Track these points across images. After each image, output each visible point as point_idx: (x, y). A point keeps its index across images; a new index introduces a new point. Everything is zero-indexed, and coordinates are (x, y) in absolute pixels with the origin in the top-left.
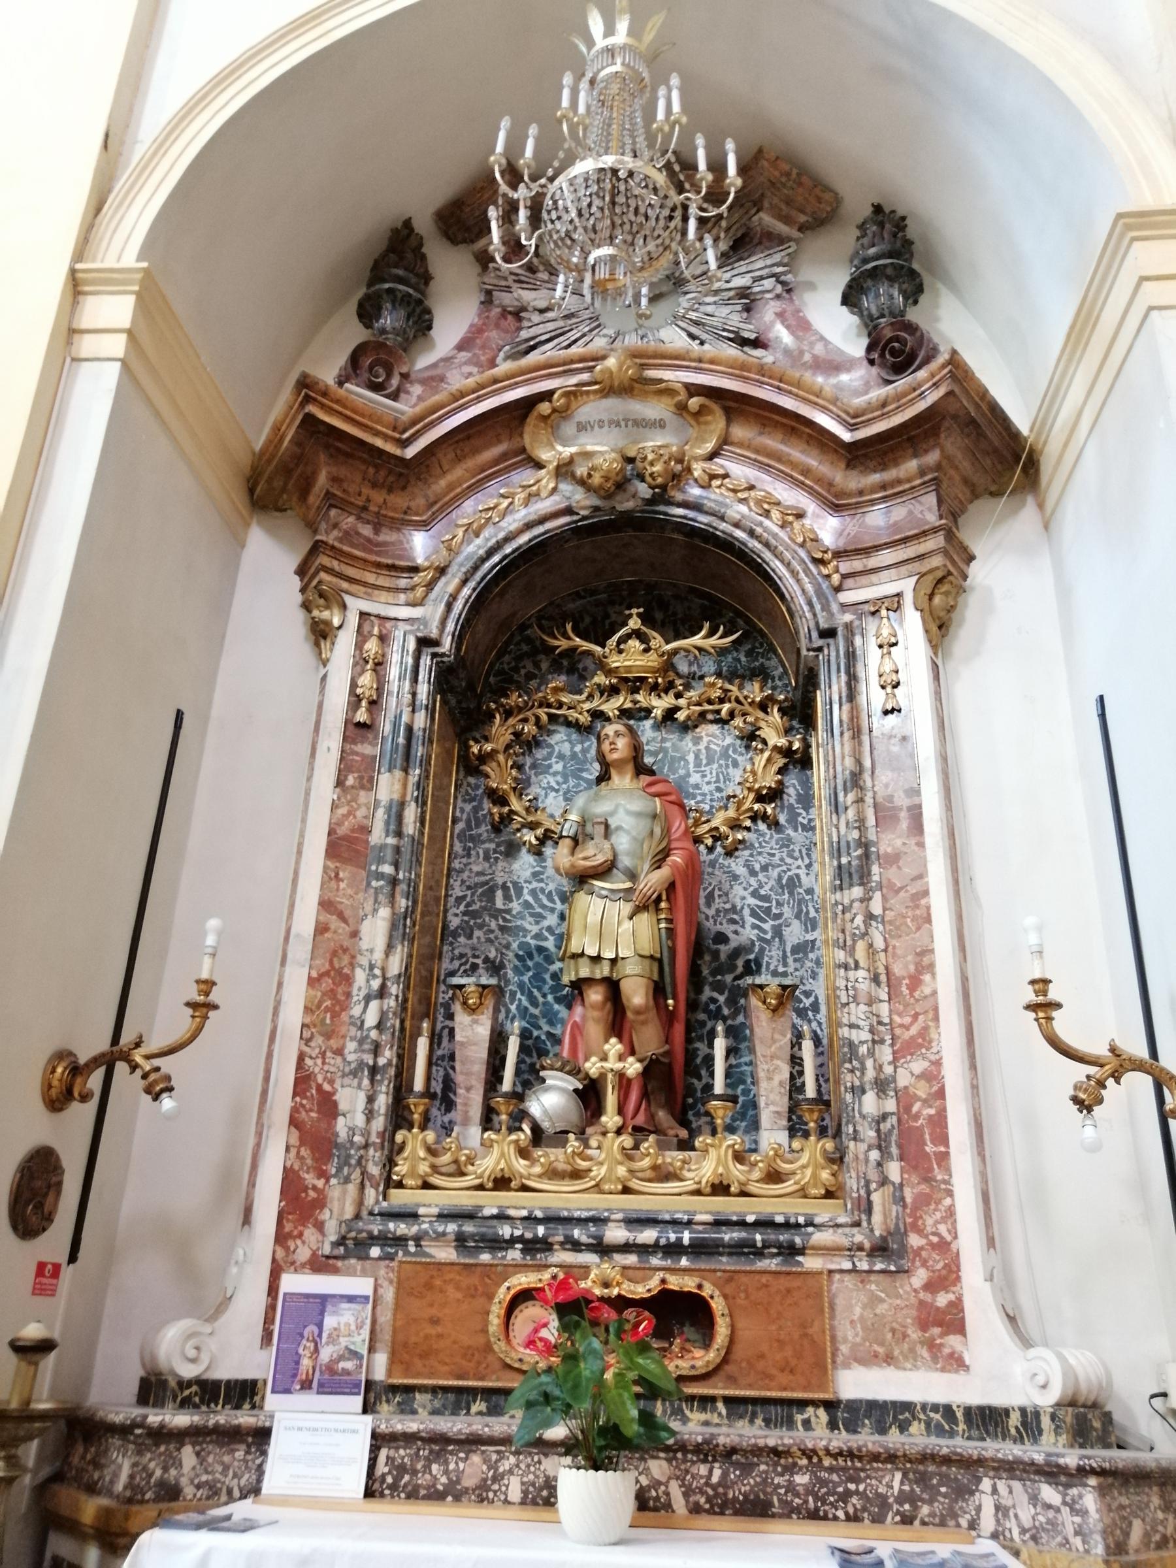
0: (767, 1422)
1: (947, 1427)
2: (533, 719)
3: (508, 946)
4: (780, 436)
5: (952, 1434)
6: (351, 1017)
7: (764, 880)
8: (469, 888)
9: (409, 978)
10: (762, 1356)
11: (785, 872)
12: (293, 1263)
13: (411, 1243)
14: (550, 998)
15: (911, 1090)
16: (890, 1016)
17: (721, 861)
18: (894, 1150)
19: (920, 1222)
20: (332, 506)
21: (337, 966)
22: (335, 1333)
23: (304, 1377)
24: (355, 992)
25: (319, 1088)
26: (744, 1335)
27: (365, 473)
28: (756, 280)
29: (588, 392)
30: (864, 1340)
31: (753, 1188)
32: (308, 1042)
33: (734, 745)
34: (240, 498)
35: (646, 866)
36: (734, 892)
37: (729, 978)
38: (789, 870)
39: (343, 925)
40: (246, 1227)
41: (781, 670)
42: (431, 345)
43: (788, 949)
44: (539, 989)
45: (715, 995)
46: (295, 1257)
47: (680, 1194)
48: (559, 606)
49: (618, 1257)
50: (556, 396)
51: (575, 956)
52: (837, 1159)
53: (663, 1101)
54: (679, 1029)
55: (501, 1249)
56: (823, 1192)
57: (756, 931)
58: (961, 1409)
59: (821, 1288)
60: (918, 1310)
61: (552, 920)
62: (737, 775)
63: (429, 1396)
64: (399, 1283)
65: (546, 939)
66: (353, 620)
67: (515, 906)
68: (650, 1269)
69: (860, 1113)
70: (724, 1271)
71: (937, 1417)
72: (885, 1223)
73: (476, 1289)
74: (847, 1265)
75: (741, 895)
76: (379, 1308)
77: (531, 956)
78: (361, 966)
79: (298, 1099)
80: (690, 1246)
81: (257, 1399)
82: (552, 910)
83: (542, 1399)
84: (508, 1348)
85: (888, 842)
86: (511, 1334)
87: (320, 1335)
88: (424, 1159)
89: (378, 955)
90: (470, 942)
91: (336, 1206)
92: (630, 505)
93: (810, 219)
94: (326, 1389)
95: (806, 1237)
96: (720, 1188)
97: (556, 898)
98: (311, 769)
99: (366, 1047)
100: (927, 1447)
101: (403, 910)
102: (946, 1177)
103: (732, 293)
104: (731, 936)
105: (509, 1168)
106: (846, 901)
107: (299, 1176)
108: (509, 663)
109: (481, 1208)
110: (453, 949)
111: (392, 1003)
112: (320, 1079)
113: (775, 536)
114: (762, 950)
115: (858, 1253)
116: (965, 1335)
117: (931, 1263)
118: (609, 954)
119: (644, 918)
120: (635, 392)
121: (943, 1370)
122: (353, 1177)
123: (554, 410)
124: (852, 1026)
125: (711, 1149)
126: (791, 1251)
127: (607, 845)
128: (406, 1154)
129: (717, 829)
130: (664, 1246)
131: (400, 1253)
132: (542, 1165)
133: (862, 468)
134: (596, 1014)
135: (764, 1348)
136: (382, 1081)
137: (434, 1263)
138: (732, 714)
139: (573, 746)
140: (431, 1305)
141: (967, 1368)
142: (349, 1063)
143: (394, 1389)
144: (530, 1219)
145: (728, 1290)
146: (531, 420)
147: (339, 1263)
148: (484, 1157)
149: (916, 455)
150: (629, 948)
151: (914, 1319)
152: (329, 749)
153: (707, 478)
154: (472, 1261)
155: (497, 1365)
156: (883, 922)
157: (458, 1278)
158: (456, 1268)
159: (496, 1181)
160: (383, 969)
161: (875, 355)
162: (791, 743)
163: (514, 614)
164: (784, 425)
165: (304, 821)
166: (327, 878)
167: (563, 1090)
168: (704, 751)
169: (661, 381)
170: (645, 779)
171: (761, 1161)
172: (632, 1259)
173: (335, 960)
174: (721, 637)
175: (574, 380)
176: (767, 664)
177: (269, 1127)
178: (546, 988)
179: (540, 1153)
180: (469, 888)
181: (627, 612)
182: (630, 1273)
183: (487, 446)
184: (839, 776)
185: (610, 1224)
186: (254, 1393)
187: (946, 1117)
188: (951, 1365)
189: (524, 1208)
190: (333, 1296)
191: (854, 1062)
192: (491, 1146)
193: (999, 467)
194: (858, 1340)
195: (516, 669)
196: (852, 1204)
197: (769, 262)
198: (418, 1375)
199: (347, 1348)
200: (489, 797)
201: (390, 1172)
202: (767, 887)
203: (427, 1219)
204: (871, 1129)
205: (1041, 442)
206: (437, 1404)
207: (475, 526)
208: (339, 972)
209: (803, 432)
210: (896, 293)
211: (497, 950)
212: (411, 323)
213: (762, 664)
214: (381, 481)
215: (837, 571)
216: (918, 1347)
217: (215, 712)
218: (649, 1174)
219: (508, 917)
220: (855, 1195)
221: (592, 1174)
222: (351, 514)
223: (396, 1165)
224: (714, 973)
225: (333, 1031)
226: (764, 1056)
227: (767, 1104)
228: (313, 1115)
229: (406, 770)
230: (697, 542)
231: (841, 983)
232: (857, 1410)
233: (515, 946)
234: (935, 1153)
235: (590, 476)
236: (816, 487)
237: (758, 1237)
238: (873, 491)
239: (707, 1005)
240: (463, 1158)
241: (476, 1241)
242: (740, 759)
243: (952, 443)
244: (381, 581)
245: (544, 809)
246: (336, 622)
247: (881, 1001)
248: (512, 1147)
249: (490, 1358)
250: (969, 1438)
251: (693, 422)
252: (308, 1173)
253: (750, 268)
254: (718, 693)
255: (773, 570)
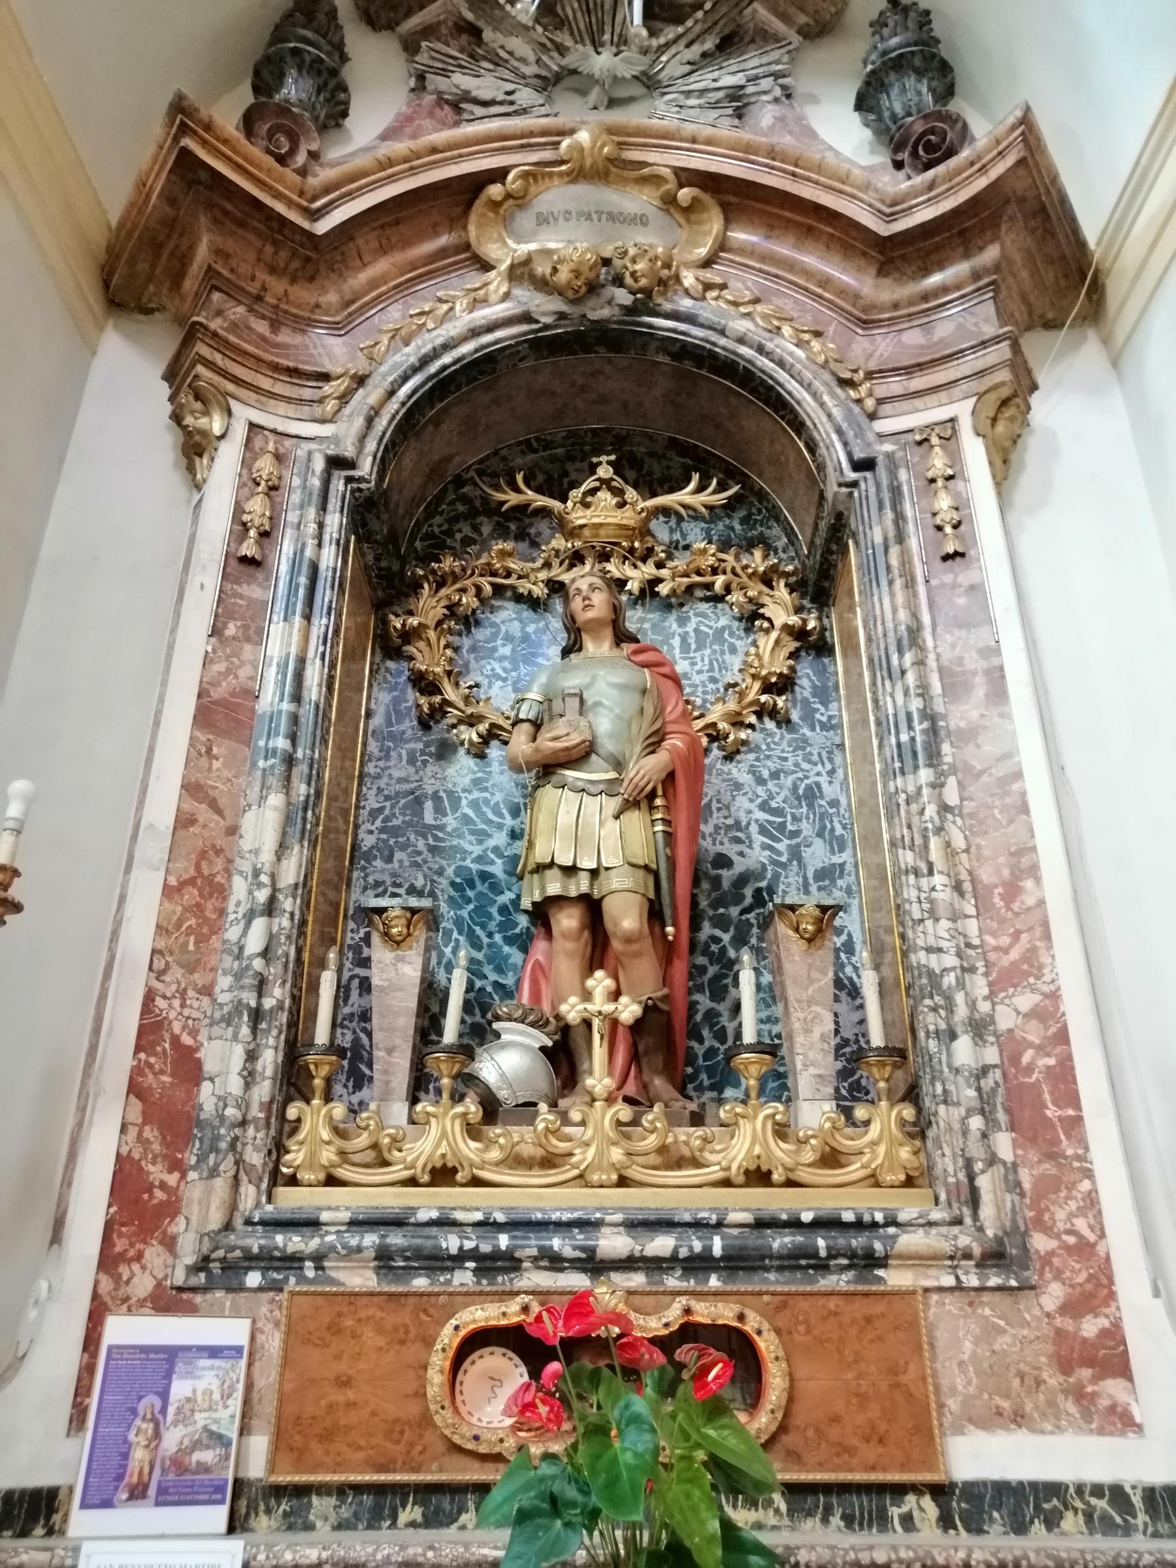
0: (849, 1520)
1: (1118, 1520)
2: (473, 591)
3: (440, 872)
4: (792, 240)
5: (1127, 1530)
6: (225, 942)
7: (774, 789)
8: (387, 798)
9: (310, 892)
10: (835, 1419)
11: (801, 780)
12: (126, 1299)
13: (309, 1264)
14: (498, 938)
15: (1018, 1034)
16: (980, 936)
17: (718, 766)
18: (1001, 1116)
19: (1046, 1217)
20: (215, 288)
21: (206, 872)
22: (188, 1406)
23: (135, 1479)
24: (231, 907)
25: (175, 1040)
26: (809, 1388)
27: (260, 251)
28: (754, 79)
29: (551, 175)
30: (981, 1389)
31: (803, 1175)
32: (160, 975)
33: (730, 627)
34: (94, 298)
35: (638, 749)
36: (737, 804)
37: (734, 911)
38: (807, 777)
39: (216, 817)
40: (55, 1246)
41: (785, 540)
42: (349, 139)
43: (810, 875)
44: (483, 926)
45: (718, 932)
46: (129, 1290)
47: (700, 1186)
48: (504, 459)
49: (617, 1277)
50: (510, 177)
51: (540, 868)
52: (919, 1130)
53: (661, 1067)
54: (680, 968)
55: (444, 1269)
56: (902, 1177)
57: (767, 853)
58: (1139, 1492)
59: (915, 1314)
60: (1055, 1343)
61: (499, 839)
62: (736, 662)
63: (333, 1501)
64: (289, 1325)
65: (492, 863)
66: (239, 431)
67: (451, 822)
68: (664, 1293)
69: (949, 1066)
70: (774, 1294)
71: (1101, 1504)
72: (999, 1218)
73: (407, 1332)
74: (948, 1281)
75: (745, 808)
76: (257, 1364)
77: (472, 886)
78: (241, 873)
79: (142, 1056)
80: (723, 1258)
81: (56, 1518)
82: (500, 827)
83: (545, 1506)
84: (457, 1420)
85: (958, 716)
86: (459, 1398)
87: (164, 1411)
88: (328, 1143)
89: (267, 857)
90: (389, 866)
91: (194, 1212)
92: (605, 313)
93: (811, 22)
94: (167, 1497)
95: (890, 1242)
96: (759, 1177)
97: (505, 811)
98: (177, 614)
99: (247, 981)
100: (1118, 1555)
101: (302, 798)
102: (1080, 1152)
103: (721, 94)
104: (736, 858)
105: (454, 1154)
106: (911, 789)
107: (141, 1169)
108: (440, 526)
109: (413, 1210)
110: (366, 876)
111: (286, 923)
112: (177, 1027)
113: (791, 354)
114: (776, 876)
115: (963, 1263)
116: (1130, 1379)
117: (1068, 1274)
118: (589, 863)
119: (635, 819)
120: (612, 177)
121: (1101, 1432)
122: (222, 1168)
123: (509, 196)
124: (929, 950)
125: (741, 1121)
126: (869, 1262)
127: (583, 723)
128: (301, 1136)
129: (713, 725)
130: (686, 1259)
131: (292, 1280)
132: (501, 1147)
133: (897, 275)
134: (570, 945)
135: (838, 1406)
136: (269, 1030)
137: (343, 1294)
138: (728, 589)
139: (524, 625)
140: (338, 1357)
141: (1138, 1428)
142: (221, 1005)
143: (278, 1491)
144: (487, 1225)
145: (782, 1321)
146: (478, 207)
147: (198, 1299)
148: (416, 1140)
149: (967, 255)
150: (616, 856)
151: (1049, 1357)
152: (202, 586)
153: (700, 287)
154: (400, 1289)
155: (440, 1447)
156: (961, 815)
157: (379, 1314)
158: (376, 1299)
159: (433, 1171)
160: (273, 876)
161: (905, 156)
162: (805, 621)
163: (448, 459)
164: (797, 224)
165: (164, 683)
166: (194, 753)
167: (526, 1048)
168: (692, 634)
169: (644, 164)
170: (628, 648)
171: (813, 1137)
172: (637, 1280)
173: (204, 865)
174: (714, 493)
175: (534, 157)
176: (767, 532)
177: (97, 1096)
178: (492, 926)
179: (498, 1131)
180: (387, 798)
181: (595, 460)
182: (637, 1300)
183: (421, 237)
184: (891, 634)
185: (604, 1230)
186: (51, 1510)
187: (1072, 1068)
188: (1114, 1424)
189: (477, 1209)
190: (187, 1349)
191: (937, 998)
192: (428, 1123)
193: (1063, 283)
194: (972, 1390)
195: (450, 533)
196: (948, 1193)
197: (765, 60)
198: (316, 1468)
199: (205, 1429)
200: (414, 686)
201: (277, 1162)
202: (779, 799)
203: (333, 1229)
204: (970, 1087)
205: (1111, 258)
206: (346, 1512)
207: (403, 332)
208: (210, 880)
209: (821, 232)
210: (925, 90)
211: (425, 877)
212: (321, 98)
213: (761, 533)
214: (282, 265)
215: (870, 395)
216: (1060, 1398)
217: (48, 549)
218: (654, 1159)
219: (441, 835)
220: (951, 1180)
221: (574, 1159)
222: (240, 303)
223: (288, 1152)
224: (715, 905)
225: (198, 961)
226: (798, 1001)
227: (805, 1065)
228: (166, 1079)
229: (308, 617)
230: (688, 365)
231: (912, 894)
232: (981, 1498)
233: (450, 871)
234: (1060, 1118)
235: (555, 270)
236: (838, 301)
237: (821, 1243)
238: (911, 303)
239: (707, 945)
240: (387, 1140)
241: (407, 1259)
242: (738, 643)
243: (1013, 241)
244: (279, 389)
245: (489, 699)
246: (217, 428)
247: (967, 916)
248: (457, 1122)
249: (429, 1437)
250: (1156, 1535)
251: (682, 221)
252: (154, 1163)
253: (742, 66)
254: (711, 561)
255: (789, 393)
